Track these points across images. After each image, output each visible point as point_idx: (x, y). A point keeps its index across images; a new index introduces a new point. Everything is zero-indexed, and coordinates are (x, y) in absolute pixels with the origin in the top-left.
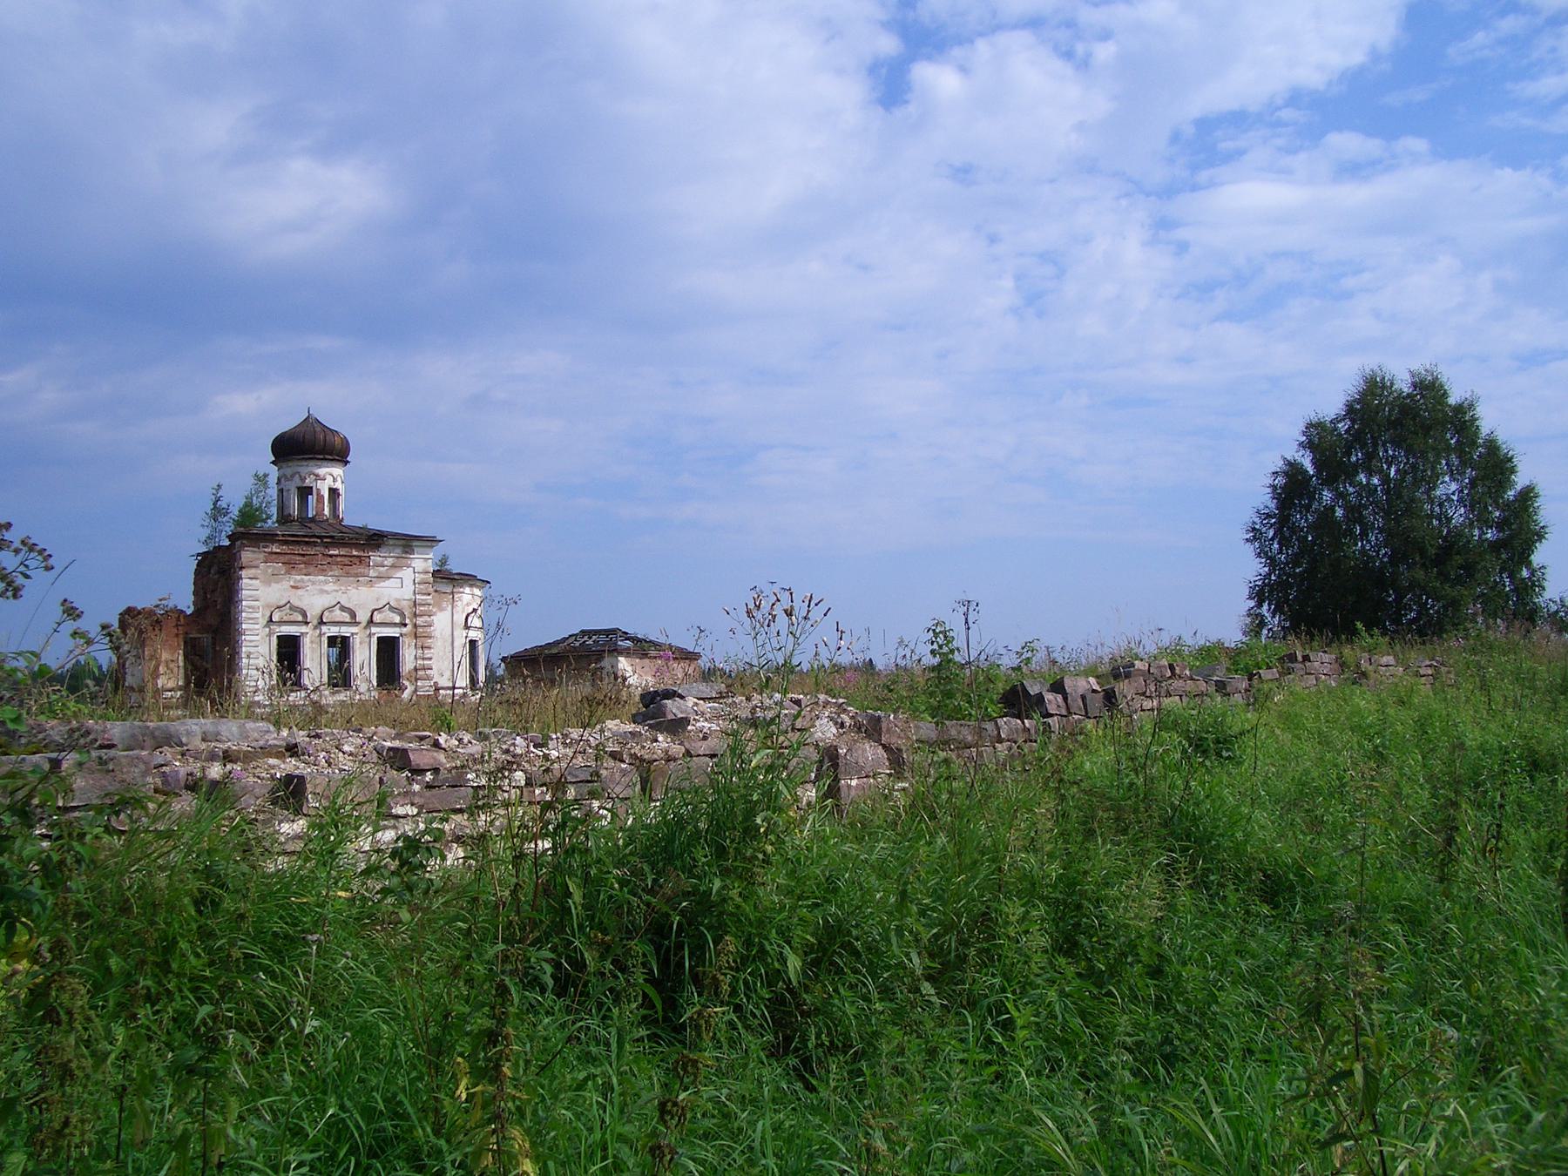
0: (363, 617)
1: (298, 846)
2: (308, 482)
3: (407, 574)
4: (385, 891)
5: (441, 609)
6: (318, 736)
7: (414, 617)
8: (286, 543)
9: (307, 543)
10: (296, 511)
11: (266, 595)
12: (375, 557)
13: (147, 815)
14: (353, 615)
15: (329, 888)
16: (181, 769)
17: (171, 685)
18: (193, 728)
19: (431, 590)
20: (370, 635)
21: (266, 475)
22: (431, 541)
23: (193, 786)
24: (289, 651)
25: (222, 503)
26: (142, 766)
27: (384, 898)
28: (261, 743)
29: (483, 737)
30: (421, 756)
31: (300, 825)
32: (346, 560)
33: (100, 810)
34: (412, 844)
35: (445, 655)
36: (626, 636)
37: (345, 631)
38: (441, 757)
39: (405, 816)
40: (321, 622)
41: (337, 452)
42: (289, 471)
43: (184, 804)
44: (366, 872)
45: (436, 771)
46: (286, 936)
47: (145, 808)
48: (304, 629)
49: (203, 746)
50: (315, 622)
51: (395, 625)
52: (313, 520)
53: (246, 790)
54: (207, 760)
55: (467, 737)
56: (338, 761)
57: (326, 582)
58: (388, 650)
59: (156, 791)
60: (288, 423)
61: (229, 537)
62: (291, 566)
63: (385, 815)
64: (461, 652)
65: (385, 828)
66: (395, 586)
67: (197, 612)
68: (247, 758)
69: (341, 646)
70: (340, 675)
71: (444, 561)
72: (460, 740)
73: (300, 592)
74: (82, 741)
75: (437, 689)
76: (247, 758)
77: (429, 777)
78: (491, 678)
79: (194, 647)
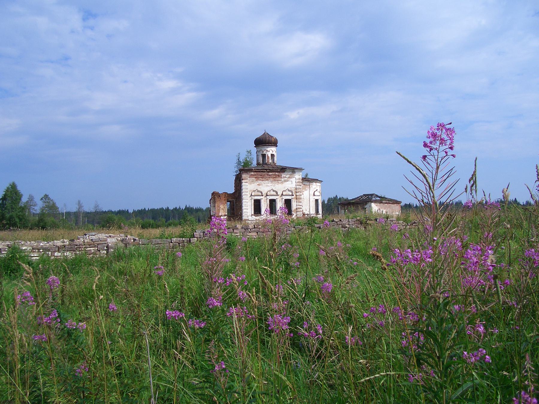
0: (280, 193)
2: (264, 153)
3: (293, 180)
5: (306, 190)
7: (296, 193)
8: (256, 172)
11: (250, 187)
12: (283, 175)
14: (277, 193)
17: (223, 214)
22: (301, 169)
32: (274, 176)
35: (308, 202)
36: (377, 196)
40: (267, 195)
41: (274, 143)
42: (259, 150)
51: (290, 195)
58: (288, 203)
60: (259, 134)
64: (313, 204)
66: (287, 185)
69: (272, 203)
71: (307, 175)
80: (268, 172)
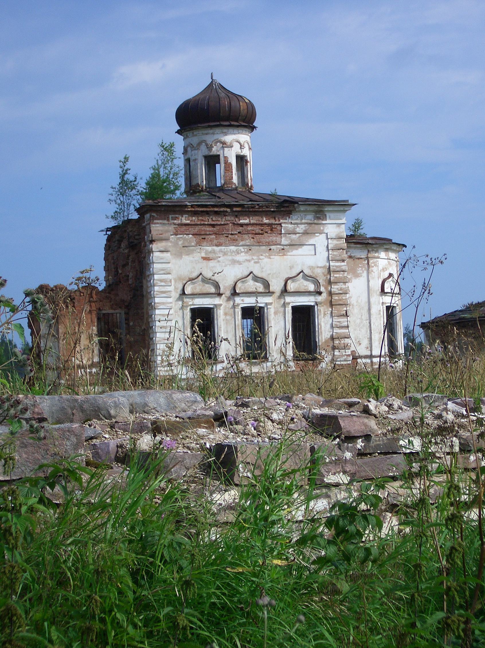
0: (276, 286)
1: (231, 517)
2: (215, 150)
3: (320, 241)
4: (322, 561)
5: (357, 276)
6: (245, 405)
7: (329, 285)
8: (195, 213)
9: (217, 213)
10: (205, 180)
11: (176, 267)
12: (287, 225)
13: (81, 488)
14: (266, 284)
15: (264, 558)
16: (111, 441)
18: (121, 400)
19: (345, 256)
20: (284, 305)
21: (172, 145)
22: (343, 205)
23: (124, 458)
24: (203, 320)
25: (129, 177)
26: (74, 439)
27: (320, 569)
28: (190, 413)
29: (414, 403)
30: (352, 423)
31: (231, 496)
32: (257, 229)
33: (34, 483)
34: (348, 511)
35: (362, 322)
37: (262, 301)
38: (372, 423)
39: (337, 485)
40: (234, 294)
41: (242, 118)
42: (195, 140)
43: (115, 476)
44: (302, 541)
45: (367, 437)
46: (224, 606)
47: (78, 480)
48: (217, 301)
49: (131, 418)
50: (228, 293)
52: (221, 189)
53: (179, 461)
54: (133, 431)
55: (397, 403)
56: (269, 429)
57: (238, 253)
58: (303, 320)
59: (88, 464)
60: (192, 90)
61: (137, 210)
62: (201, 237)
63: (316, 484)
64: (379, 321)
65: (318, 497)
66: (305, 254)
67: (110, 287)
68: (173, 429)
69: (254, 315)
70: (255, 346)
71: (357, 225)
72: (390, 406)
73: (212, 263)
74: (12, 411)
75: (355, 358)
76: (173, 429)
77: (360, 444)
78: (413, 348)
79: (107, 323)
80: (237, 215)
